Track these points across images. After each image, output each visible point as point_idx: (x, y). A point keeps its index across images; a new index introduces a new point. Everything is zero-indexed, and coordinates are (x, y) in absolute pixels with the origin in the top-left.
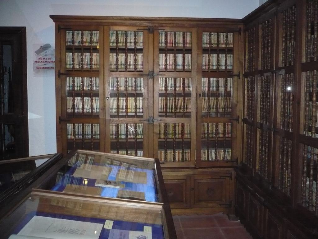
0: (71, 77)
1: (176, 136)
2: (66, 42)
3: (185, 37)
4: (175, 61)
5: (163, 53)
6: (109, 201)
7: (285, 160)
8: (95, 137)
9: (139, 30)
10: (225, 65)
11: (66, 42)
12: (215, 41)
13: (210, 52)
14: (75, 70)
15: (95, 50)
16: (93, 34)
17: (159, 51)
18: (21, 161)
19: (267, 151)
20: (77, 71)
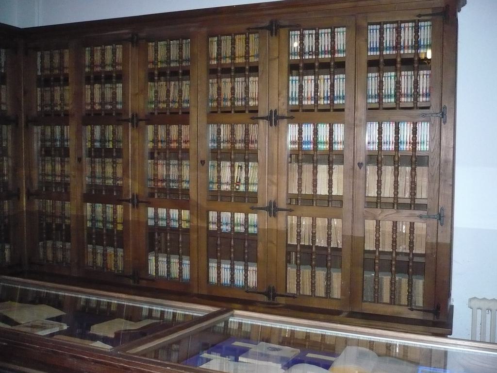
0: (310, 123)
1: (10, 164)
2: (289, 54)
3: (249, 44)
4: (301, 87)
5: (408, 70)
6: (157, 300)
7: (180, 239)
8: (239, 228)
9: (422, 18)
10: (395, 95)
11: (289, 54)
12: (229, 53)
13: (233, 74)
14: (304, 108)
15: (340, 66)
16: (221, 42)
17: (189, 71)
18: (459, 351)
19: (232, 243)
20: (309, 110)
